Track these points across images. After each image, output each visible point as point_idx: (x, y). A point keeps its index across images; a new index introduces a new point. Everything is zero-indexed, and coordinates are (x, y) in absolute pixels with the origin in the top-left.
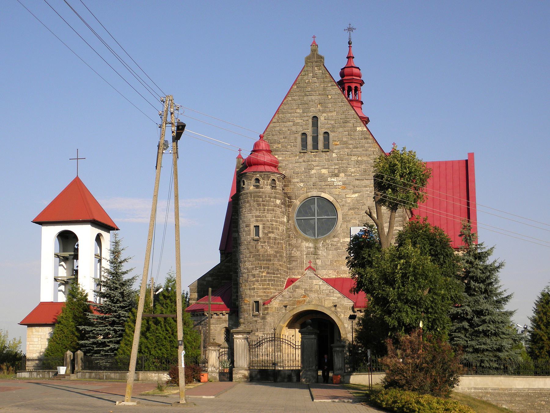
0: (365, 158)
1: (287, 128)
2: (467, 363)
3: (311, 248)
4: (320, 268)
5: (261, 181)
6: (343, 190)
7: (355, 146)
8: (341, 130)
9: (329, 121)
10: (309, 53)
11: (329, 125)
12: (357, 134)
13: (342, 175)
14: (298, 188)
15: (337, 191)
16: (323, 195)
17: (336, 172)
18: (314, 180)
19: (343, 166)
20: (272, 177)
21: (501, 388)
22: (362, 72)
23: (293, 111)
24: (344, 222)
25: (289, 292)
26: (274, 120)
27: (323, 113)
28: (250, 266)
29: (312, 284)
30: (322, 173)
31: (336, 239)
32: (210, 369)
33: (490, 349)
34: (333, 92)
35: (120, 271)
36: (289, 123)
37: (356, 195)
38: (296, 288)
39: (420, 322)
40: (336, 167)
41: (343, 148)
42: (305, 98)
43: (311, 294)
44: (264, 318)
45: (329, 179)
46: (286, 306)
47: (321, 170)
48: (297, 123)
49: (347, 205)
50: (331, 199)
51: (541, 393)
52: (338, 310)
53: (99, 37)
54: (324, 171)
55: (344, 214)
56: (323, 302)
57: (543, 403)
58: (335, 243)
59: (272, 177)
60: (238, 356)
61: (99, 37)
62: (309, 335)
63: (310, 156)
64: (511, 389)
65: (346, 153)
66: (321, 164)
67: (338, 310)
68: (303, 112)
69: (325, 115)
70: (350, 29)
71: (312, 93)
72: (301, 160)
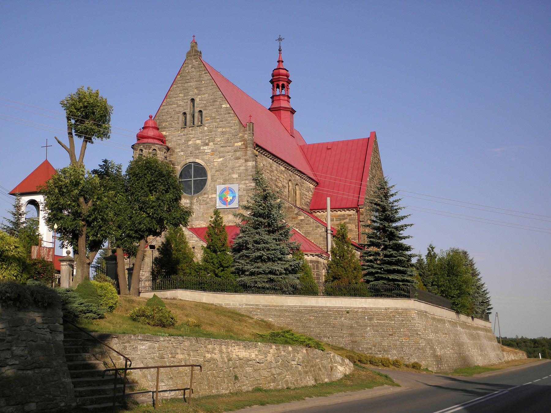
0: (228, 129)
1: (172, 110)
3: (188, 203)
4: (194, 220)
5: (144, 150)
7: (221, 120)
8: (211, 108)
9: (202, 101)
10: (189, 49)
12: (222, 110)
13: (211, 144)
14: (179, 156)
15: (206, 157)
16: (197, 161)
17: (207, 141)
18: (191, 149)
19: (212, 136)
20: (153, 147)
21: (272, 305)
22: (290, 73)
23: (176, 95)
24: (212, 181)
26: (163, 104)
27: (199, 95)
31: (206, 196)
33: (263, 272)
34: (206, 78)
35: (21, 221)
36: (174, 105)
37: (221, 159)
40: (207, 137)
41: (212, 122)
42: (186, 85)
48: (179, 105)
49: (215, 167)
51: (312, 310)
52: (196, 251)
54: (198, 142)
55: (212, 175)
57: (312, 318)
58: (205, 199)
59: (153, 147)
60: (63, 279)
62: (111, 261)
63: (188, 130)
64: (282, 306)
66: (196, 136)
67: (196, 251)
68: (184, 96)
69: (199, 97)
70: (280, 39)
71: (190, 81)
72: (182, 134)
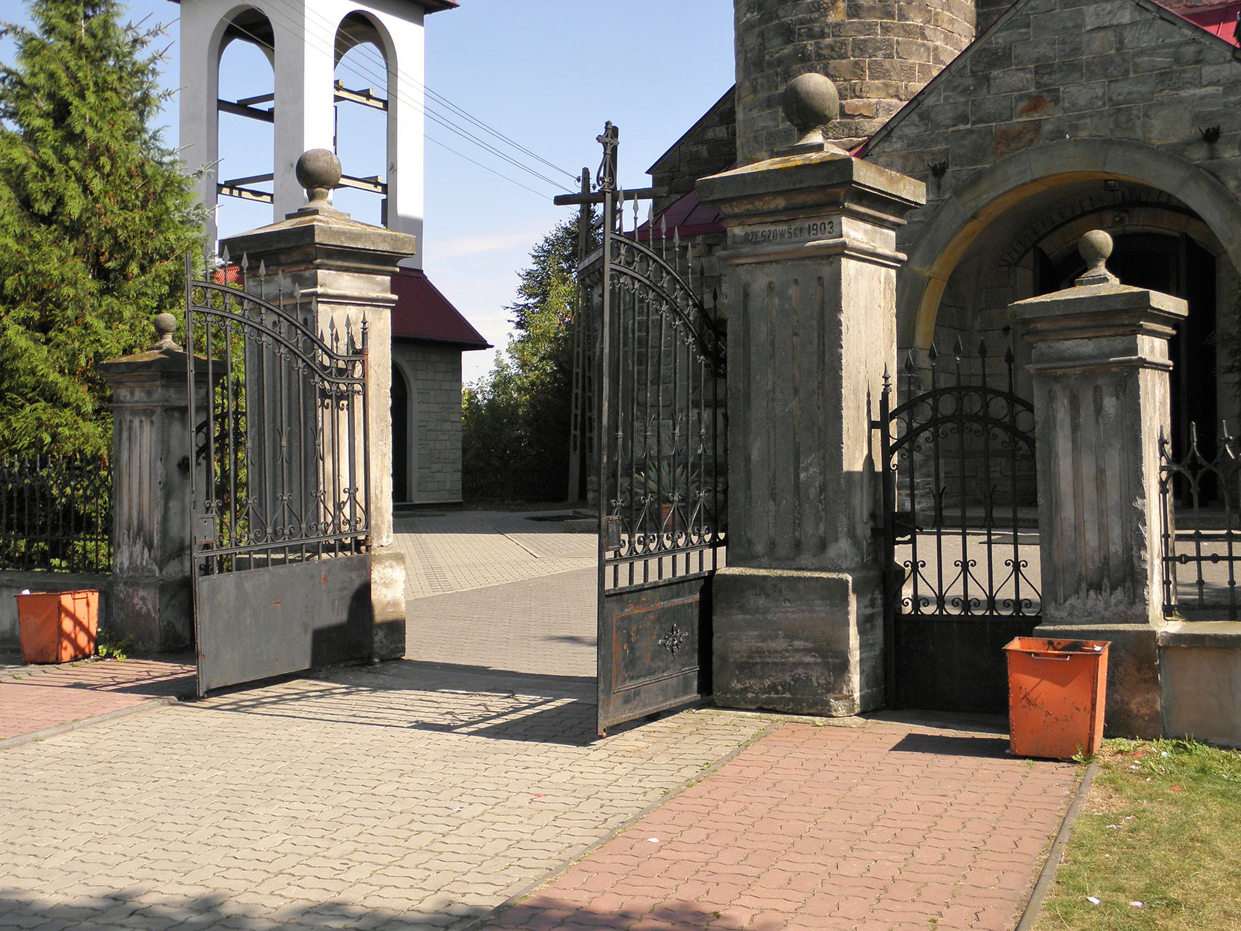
2: (21, 492)
25: (954, 89)
29: (1077, 26)
32: (126, 554)
38: (992, 65)
39: (1031, 387)
43: (1072, 89)
53: (543, 178)
56: (1138, 123)
61: (543, 178)
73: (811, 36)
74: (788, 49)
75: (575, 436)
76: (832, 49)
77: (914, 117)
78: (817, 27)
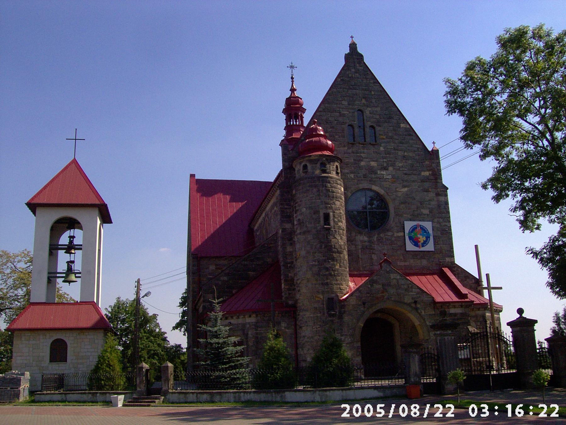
0: (411, 154)
3: (366, 242)
6: (393, 183)
11: (374, 119)
13: (391, 168)
17: (385, 165)
27: (367, 106)
28: (321, 258)
30: (371, 165)
31: (390, 234)
37: (406, 189)
40: (385, 160)
42: (350, 92)
44: (341, 317)
45: (379, 172)
46: (364, 304)
47: (369, 162)
50: (382, 192)
65: (393, 147)
68: (349, 104)
69: (370, 109)
72: (350, 151)
73: (333, 270)
74: (327, 273)
75: (155, 402)
76: (337, 274)
77: (358, 292)
78: (334, 269)
